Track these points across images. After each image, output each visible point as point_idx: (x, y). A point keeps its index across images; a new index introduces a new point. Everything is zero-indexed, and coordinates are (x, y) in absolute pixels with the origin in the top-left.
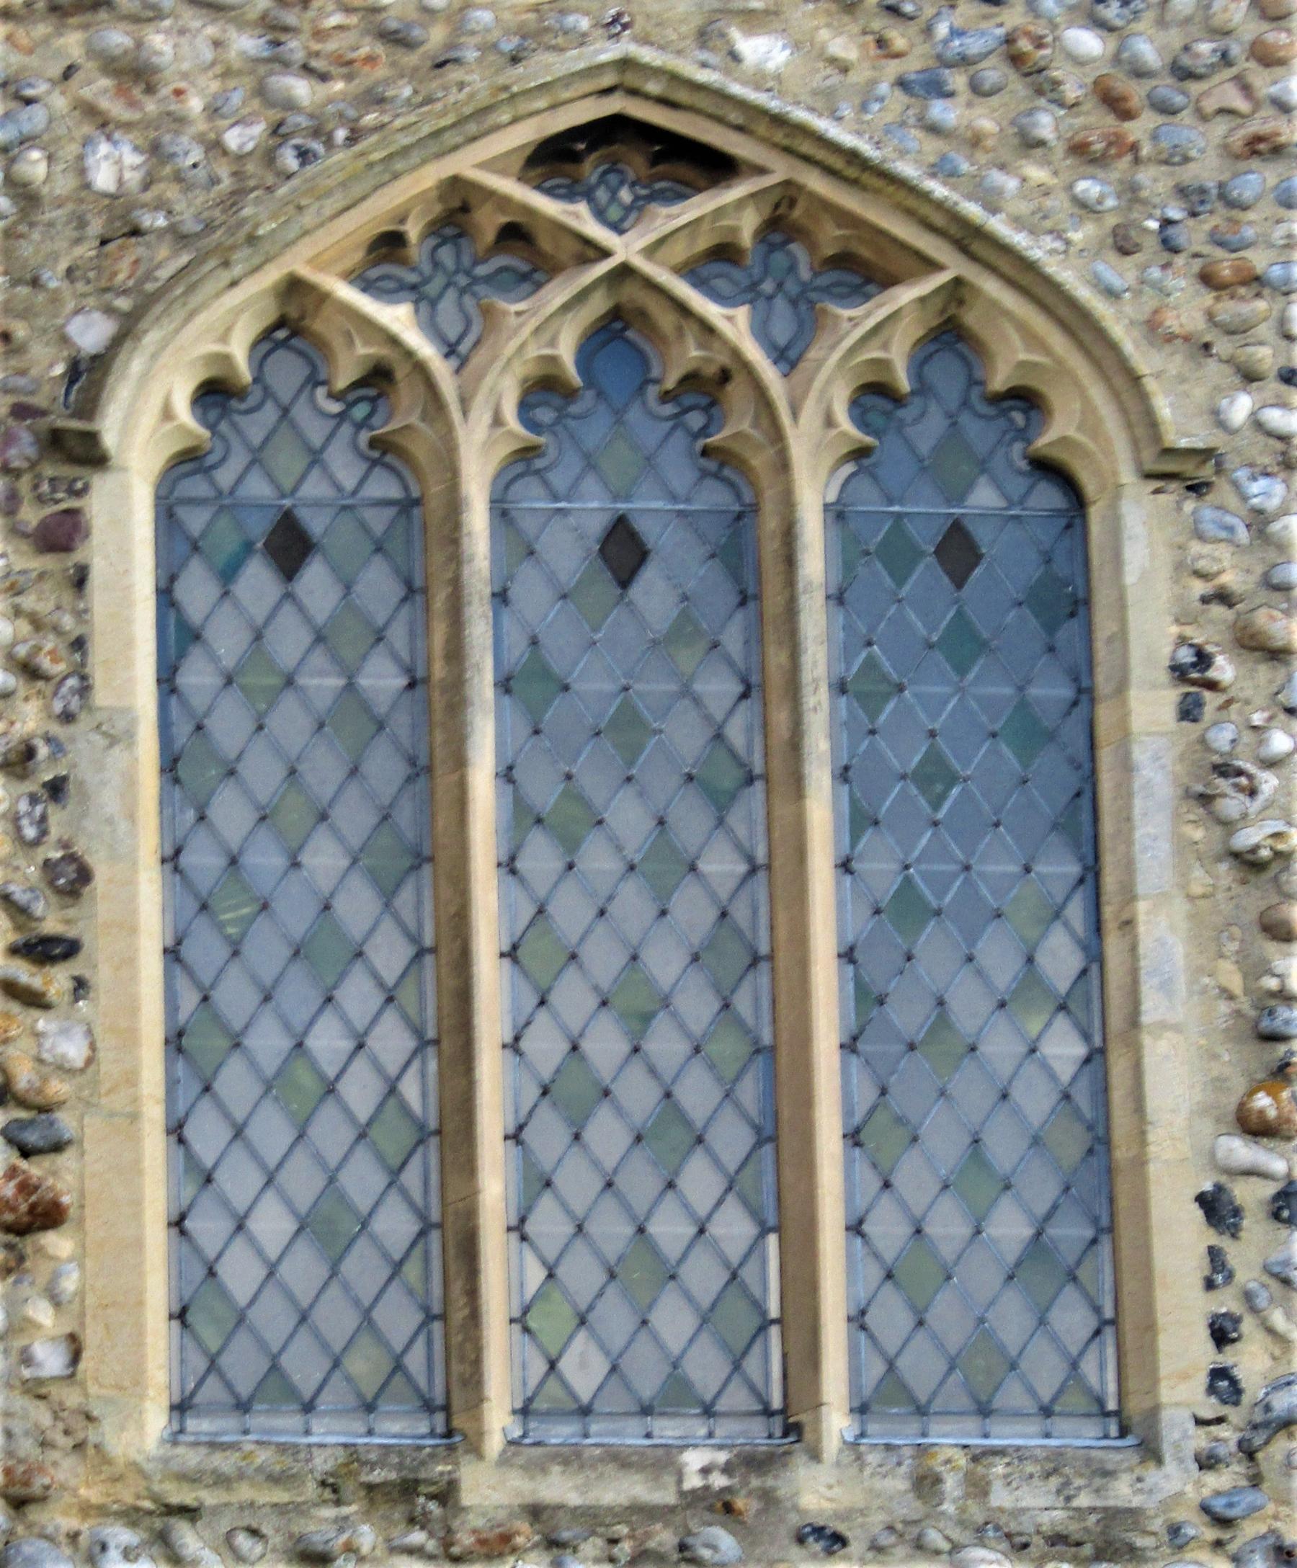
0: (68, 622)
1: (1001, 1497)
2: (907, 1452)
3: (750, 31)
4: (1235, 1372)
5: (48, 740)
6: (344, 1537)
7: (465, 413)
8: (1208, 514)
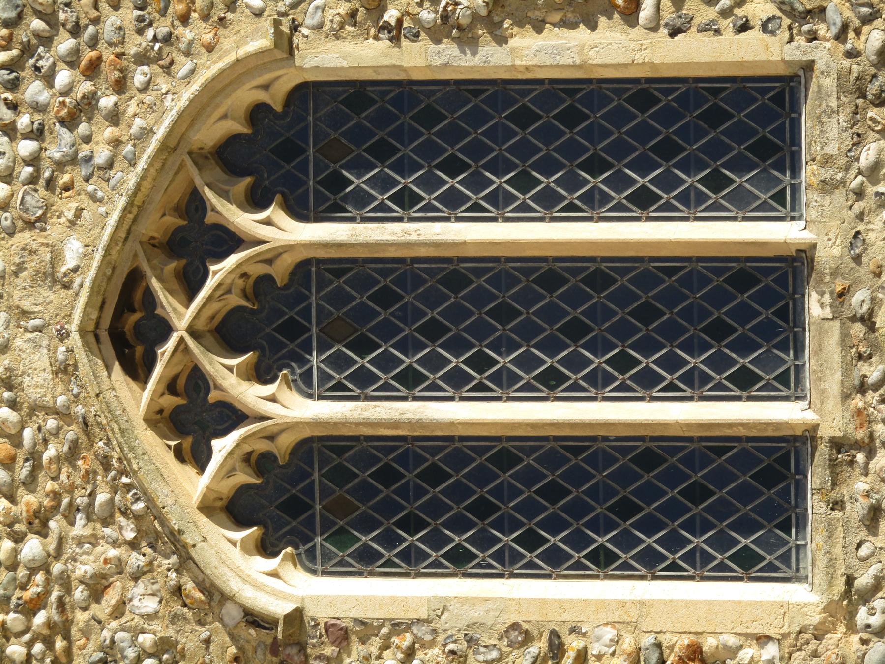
0: (385, 630)
1: (832, 149)
2: (810, 195)
3: (64, 262)
4: (764, 20)
5: (445, 645)
6: (861, 499)
7: (269, 418)
8: (309, 21)
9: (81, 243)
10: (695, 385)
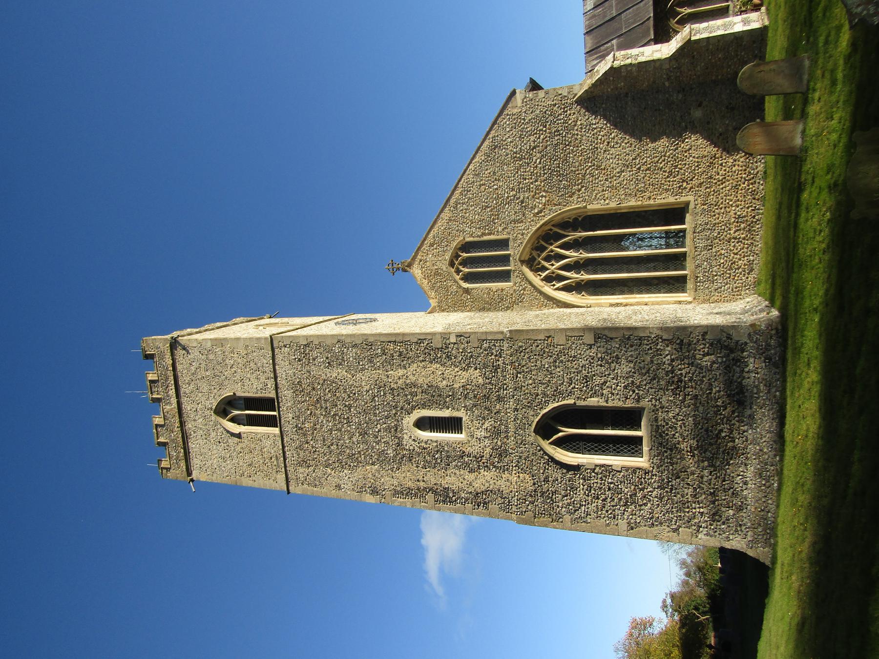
9: (448, 257)
10: (501, 266)
